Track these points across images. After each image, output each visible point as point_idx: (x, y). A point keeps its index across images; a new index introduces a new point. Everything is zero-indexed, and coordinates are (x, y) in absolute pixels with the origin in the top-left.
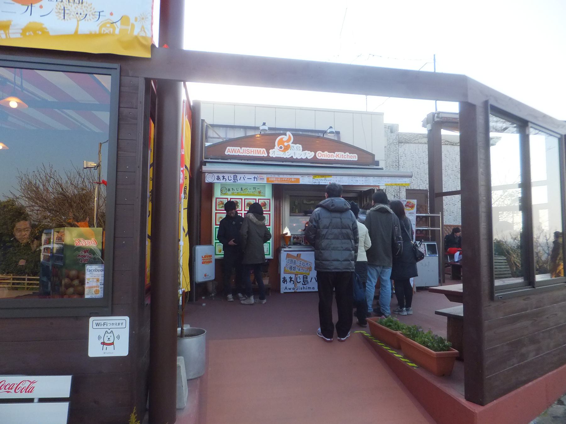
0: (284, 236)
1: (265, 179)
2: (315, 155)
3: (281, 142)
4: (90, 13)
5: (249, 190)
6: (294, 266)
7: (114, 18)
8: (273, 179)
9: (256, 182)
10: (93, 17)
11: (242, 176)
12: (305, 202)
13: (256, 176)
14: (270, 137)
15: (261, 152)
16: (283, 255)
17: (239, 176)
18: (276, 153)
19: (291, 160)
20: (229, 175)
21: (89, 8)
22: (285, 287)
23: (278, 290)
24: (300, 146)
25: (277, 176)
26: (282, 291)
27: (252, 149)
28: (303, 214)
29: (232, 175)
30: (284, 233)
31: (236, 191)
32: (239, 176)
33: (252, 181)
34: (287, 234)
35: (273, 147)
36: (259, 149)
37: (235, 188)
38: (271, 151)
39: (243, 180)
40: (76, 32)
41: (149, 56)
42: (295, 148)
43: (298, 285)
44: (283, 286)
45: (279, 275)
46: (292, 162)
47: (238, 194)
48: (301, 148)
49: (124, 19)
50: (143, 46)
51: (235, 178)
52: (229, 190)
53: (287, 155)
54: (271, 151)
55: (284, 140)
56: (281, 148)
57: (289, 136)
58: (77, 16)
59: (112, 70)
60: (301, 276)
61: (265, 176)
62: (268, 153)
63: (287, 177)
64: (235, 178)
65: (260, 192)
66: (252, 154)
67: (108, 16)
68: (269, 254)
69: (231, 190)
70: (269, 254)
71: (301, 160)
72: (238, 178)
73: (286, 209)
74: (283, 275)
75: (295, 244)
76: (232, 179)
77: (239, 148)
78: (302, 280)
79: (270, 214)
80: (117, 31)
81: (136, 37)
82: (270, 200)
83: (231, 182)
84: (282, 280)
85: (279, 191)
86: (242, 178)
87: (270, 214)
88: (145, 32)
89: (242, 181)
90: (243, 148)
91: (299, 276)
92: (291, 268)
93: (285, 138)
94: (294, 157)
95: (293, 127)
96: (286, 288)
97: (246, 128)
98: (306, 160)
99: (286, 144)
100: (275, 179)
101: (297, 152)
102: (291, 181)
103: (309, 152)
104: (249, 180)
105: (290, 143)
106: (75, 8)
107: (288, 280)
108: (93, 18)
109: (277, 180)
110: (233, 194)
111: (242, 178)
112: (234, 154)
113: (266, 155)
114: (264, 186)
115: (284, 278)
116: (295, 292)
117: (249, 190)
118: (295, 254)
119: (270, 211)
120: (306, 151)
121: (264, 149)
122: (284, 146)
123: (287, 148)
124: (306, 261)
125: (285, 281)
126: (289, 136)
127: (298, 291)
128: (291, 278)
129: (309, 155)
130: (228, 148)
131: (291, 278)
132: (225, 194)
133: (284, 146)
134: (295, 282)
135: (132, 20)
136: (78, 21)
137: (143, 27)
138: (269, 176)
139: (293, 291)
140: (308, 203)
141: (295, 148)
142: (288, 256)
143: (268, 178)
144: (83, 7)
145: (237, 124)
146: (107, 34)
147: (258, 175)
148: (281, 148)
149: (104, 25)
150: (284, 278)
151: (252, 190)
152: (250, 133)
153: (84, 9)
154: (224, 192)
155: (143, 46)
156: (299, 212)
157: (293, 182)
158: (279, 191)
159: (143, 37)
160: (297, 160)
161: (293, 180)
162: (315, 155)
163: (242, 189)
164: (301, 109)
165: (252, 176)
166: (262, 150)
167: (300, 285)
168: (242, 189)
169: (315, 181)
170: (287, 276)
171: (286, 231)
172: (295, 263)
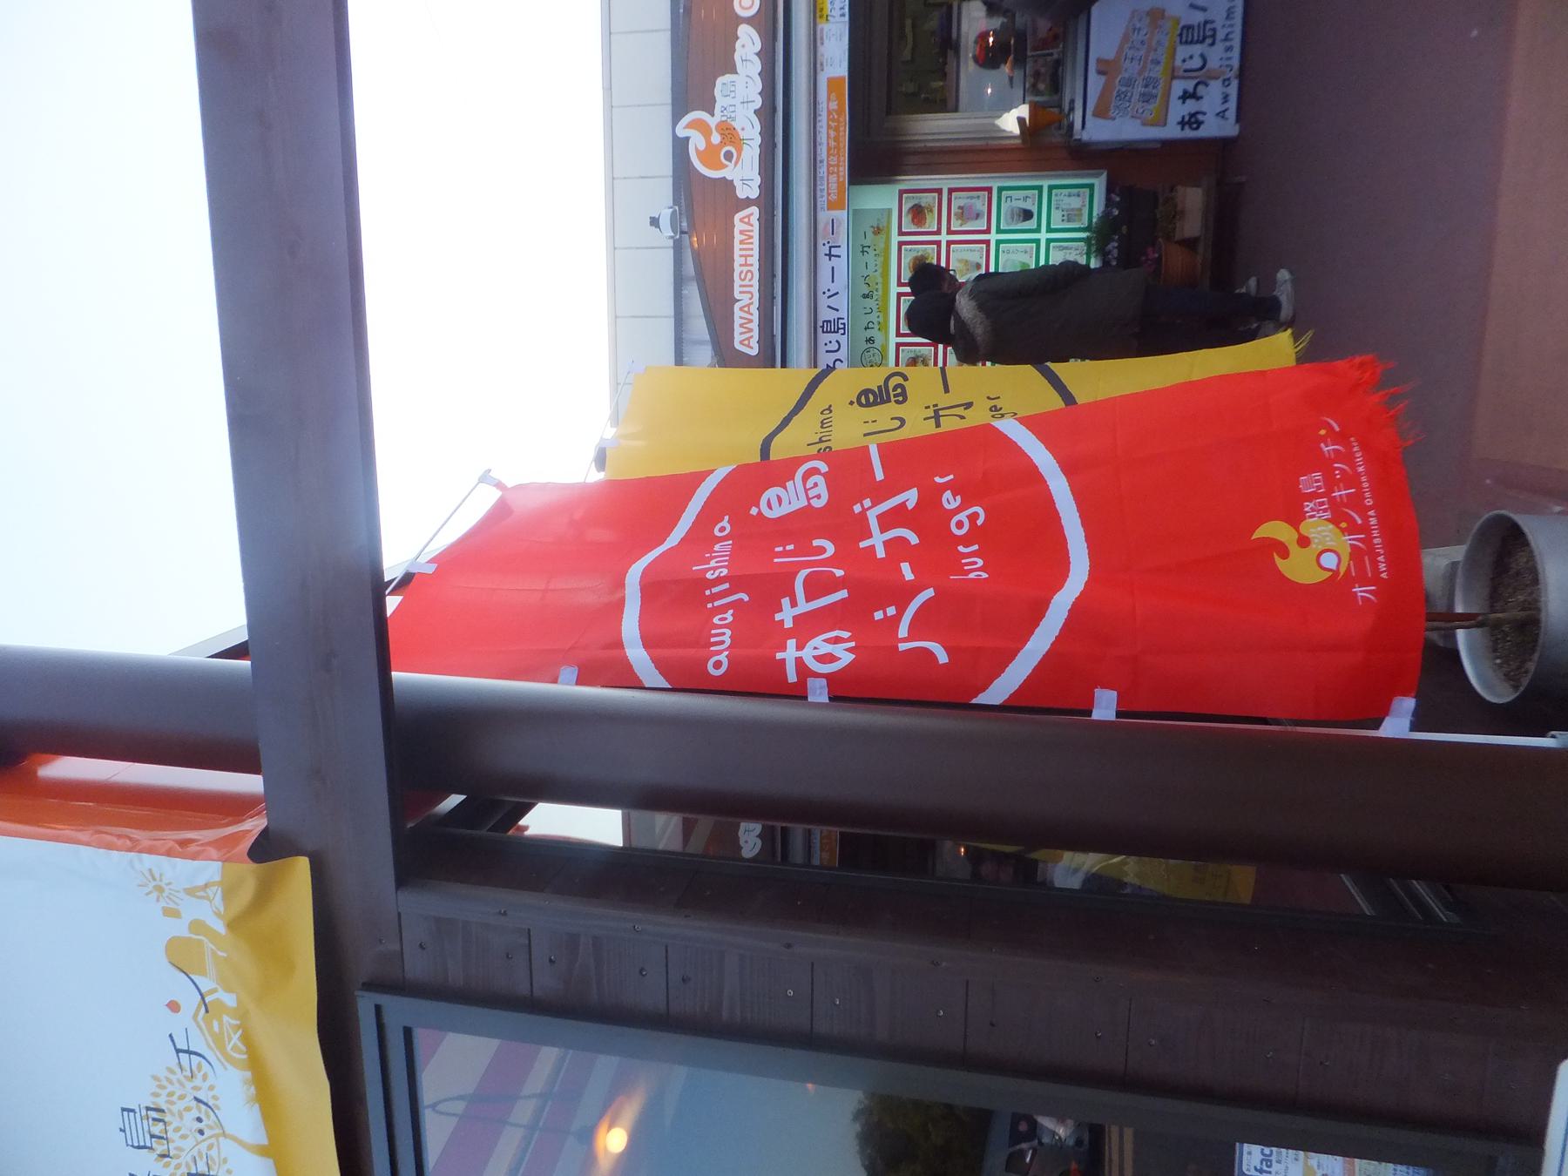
0: (1029, 130)
1: (835, 213)
2: (749, 21)
3: (709, 156)
4: (189, 1085)
5: (870, 272)
6: (1140, 82)
7: (189, 1001)
8: (834, 186)
9: (843, 251)
10: (199, 1076)
11: (823, 302)
12: (907, 54)
13: (823, 250)
14: (697, 200)
15: (746, 227)
16: (1096, 131)
17: (825, 314)
18: (745, 175)
19: (766, 114)
20: (822, 349)
21: (170, 1088)
22: (1218, 121)
23: (1223, 144)
24: (720, 81)
25: (822, 170)
26: (1230, 128)
27: (738, 260)
28: (950, 53)
29: (823, 338)
30: (1016, 130)
31: (873, 317)
32: (825, 314)
33: (841, 264)
34: (1021, 121)
35: (728, 185)
36: (738, 237)
37: (865, 320)
38: (741, 193)
39: (839, 306)
40: (263, 1151)
41: (303, 864)
42: (728, 101)
43: (1213, 63)
44: (1212, 128)
45: (1168, 145)
46: (774, 110)
47: (884, 309)
48: (728, 78)
49: (182, 957)
50: (264, 894)
51: (833, 327)
52: (870, 340)
53: (751, 131)
54: (741, 193)
55: (702, 146)
56: (729, 156)
57: (689, 126)
58: (207, 1133)
59: (387, 1019)
60: (1182, 51)
61: (824, 216)
62: (748, 202)
63: (825, 129)
64: (833, 327)
65: (878, 231)
66: (754, 260)
67: (185, 1017)
68: (1091, 187)
69: (869, 334)
70: (1091, 187)
71: (767, 75)
72: (831, 315)
73: (933, 127)
74: (1172, 131)
75: (1056, 86)
76: (833, 337)
77: (737, 306)
78: (1197, 49)
79: (951, 191)
80: (230, 1000)
81: (233, 925)
82: (901, 192)
83: (844, 340)
84: (1189, 133)
85: (875, 158)
86: (832, 302)
87: (951, 191)
88: (206, 886)
89: (842, 302)
90: (737, 295)
91: (1178, 63)
92: (1147, 98)
93: (697, 142)
94: (758, 103)
95: (666, 112)
96: (1221, 115)
97: (679, 282)
98: (767, 55)
99: (716, 138)
100: (833, 178)
101: (740, 92)
102: (840, 111)
103: (738, 44)
104: (837, 275)
105: (712, 122)
106: (184, 1137)
107: (1191, 106)
108: (205, 1078)
109: (836, 164)
110: (883, 327)
111: (832, 302)
112: (755, 326)
113: (755, 210)
114: (857, 215)
115: (1182, 123)
116: (1241, 75)
117: (871, 267)
118: (1096, 83)
119: (939, 191)
120: (737, 57)
121: (737, 217)
122: (723, 144)
123: (729, 133)
124: (1126, 38)
125: (1193, 121)
126: (689, 126)
127: (1236, 63)
128: (1186, 96)
129: (748, 43)
130: (738, 346)
131: (1186, 96)
132: (884, 356)
133: (723, 144)
134: (1202, 75)
135: (180, 928)
136: (224, 1135)
137: (190, 892)
138: (822, 201)
139: (1235, 84)
140: (910, 46)
141: (728, 101)
142: (1101, 113)
143: (832, 206)
144: (175, 1109)
145: (670, 310)
146: (246, 1039)
147: (820, 242)
148: (729, 156)
149: (219, 1041)
150: (1182, 123)
151: (870, 257)
152: (689, 268)
153: (180, 1105)
154: (878, 359)
155: (264, 894)
156: (944, 75)
157: (841, 105)
158: (875, 158)
159: (228, 895)
160: (768, 92)
161: (834, 105)
162: (749, 21)
163: (865, 296)
164: (608, 88)
165: (825, 265)
166: (739, 226)
167: (1216, 55)
168: (865, 296)
169: (836, 13)
170: (1178, 110)
171: (1010, 122)
172: (1129, 83)
